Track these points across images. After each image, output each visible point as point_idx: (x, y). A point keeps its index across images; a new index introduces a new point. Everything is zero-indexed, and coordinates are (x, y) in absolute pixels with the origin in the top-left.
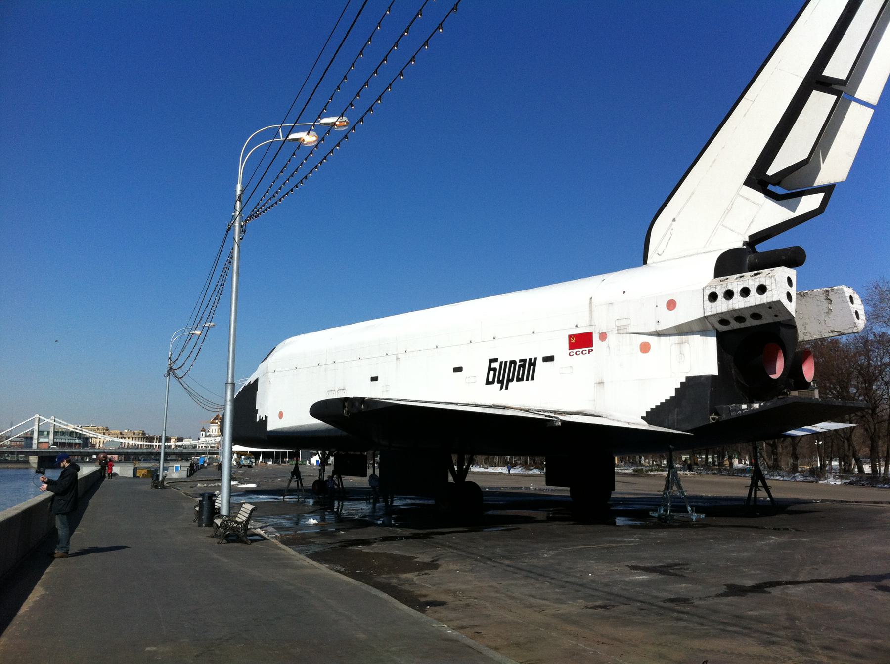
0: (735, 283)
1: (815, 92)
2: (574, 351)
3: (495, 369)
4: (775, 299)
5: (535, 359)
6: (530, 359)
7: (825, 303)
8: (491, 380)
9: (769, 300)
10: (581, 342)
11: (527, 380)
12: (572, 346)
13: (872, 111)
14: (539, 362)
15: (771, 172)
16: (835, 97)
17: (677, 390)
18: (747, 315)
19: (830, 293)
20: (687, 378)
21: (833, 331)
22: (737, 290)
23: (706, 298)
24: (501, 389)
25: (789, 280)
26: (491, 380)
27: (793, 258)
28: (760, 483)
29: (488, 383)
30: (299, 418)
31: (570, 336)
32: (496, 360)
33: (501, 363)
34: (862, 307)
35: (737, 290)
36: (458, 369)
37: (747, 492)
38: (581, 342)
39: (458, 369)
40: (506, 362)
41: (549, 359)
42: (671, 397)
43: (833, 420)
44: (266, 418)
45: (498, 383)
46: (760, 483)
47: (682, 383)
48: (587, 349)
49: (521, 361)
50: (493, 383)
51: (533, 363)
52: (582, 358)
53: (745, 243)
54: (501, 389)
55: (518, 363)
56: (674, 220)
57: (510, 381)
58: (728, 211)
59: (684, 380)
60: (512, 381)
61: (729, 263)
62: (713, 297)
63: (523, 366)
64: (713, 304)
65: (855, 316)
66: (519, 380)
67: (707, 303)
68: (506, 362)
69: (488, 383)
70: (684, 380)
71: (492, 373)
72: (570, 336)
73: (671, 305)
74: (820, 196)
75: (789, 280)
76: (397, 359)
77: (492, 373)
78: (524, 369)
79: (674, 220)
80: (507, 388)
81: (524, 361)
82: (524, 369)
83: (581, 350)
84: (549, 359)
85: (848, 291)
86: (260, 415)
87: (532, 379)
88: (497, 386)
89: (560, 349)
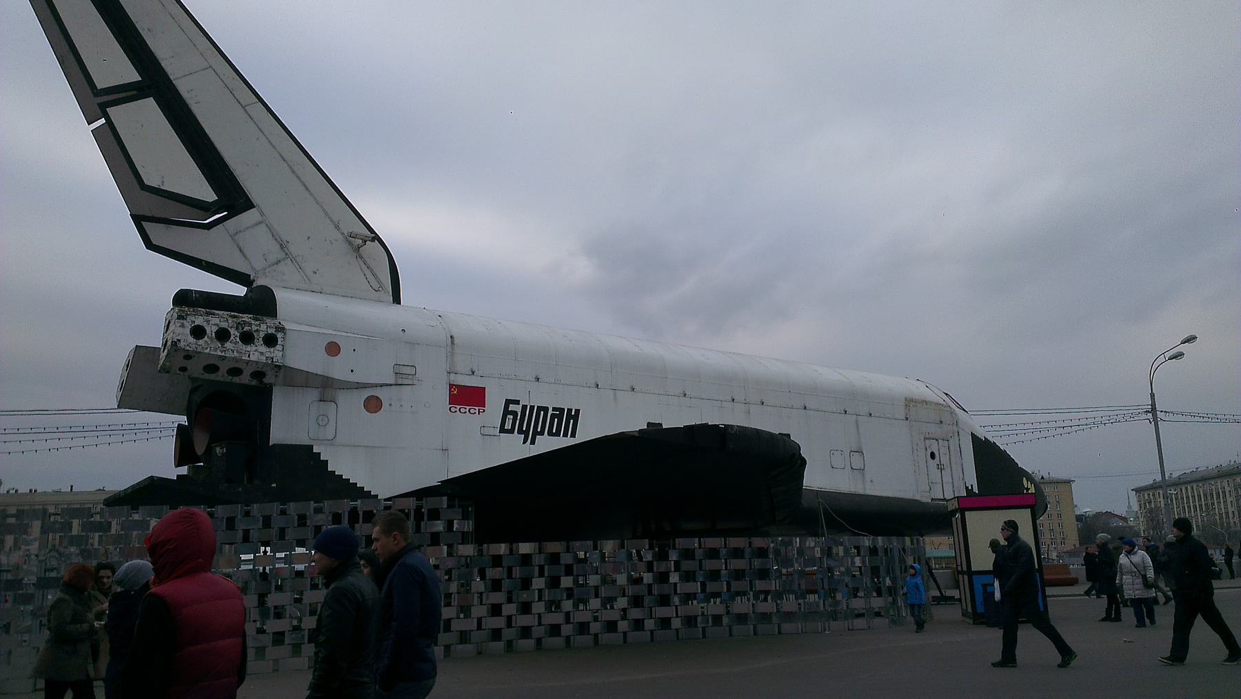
1: (151, 101)
3: (515, 413)
5: (577, 411)
6: (570, 410)
8: (508, 426)
10: (933, 456)
13: (1159, 478)
20: (804, 462)
22: (211, 330)
24: (524, 442)
26: (508, 426)
29: (503, 430)
32: (517, 402)
33: (524, 407)
35: (211, 330)
38: (933, 456)
49: (554, 409)
50: (511, 431)
54: (524, 442)
57: (536, 433)
60: (542, 433)
69: (503, 430)
73: (333, 349)
87: (1153, 621)
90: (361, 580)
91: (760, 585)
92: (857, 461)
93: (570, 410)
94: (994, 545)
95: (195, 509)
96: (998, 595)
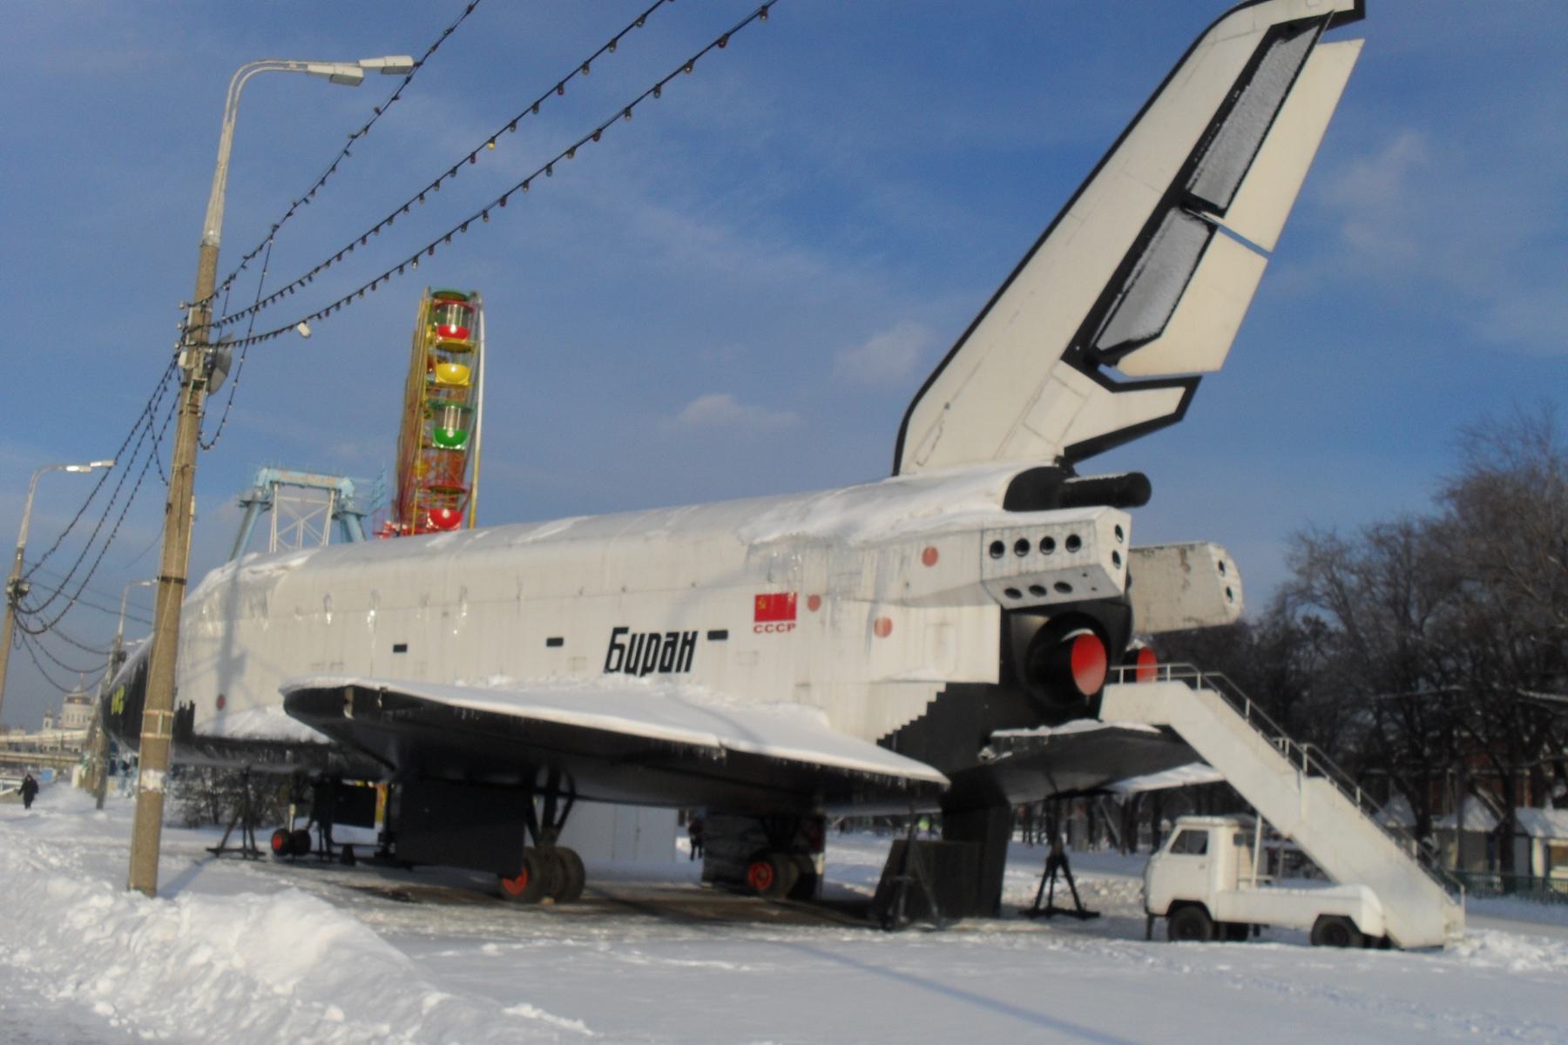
0: (1035, 523)
2: (764, 624)
3: (621, 647)
4: (1092, 561)
5: (695, 634)
6: (686, 634)
7: (1180, 571)
8: (613, 665)
9: (1084, 562)
10: (775, 609)
11: (678, 669)
12: (761, 615)
13: (1261, 262)
14: (702, 640)
15: (1104, 344)
17: (930, 705)
18: (1049, 584)
19: (1189, 553)
20: (950, 686)
21: (1190, 619)
22: (1035, 540)
23: (986, 549)
25: (1118, 531)
26: (613, 665)
27: (1127, 492)
28: (1060, 872)
29: (608, 669)
30: (262, 717)
31: (758, 598)
32: (624, 630)
33: (634, 636)
34: (1238, 582)
35: (1035, 540)
36: (555, 642)
39: (555, 642)
41: (718, 635)
42: (921, 718)
43: (1065, 736)
44: (192, 706)
46: (1060, 872)
48: (786, 623)
49: (669, 635)
51: (690, 641)
52: (774, 638)
53: (1058, 459)
55: (664, 640)
56: (947, 406)
58: (1035, 400)
61: (1029, 491)
62: (997, 548)
63: (672, 644)
64: (997, 562)
65: (1224, 594)
67: (988, 559)
68: (642, 636)
69: (608, 669)
71: (616, 653)
72: (758, 598)
74: (1178, 393)
75: (1118, 531)
76: (445, 614)
77: (616, 653)
78: (668, 653)
79: (947, 406)
81: (675, 635)
82: (668, 653)
83: (775, 623)
84: (718, 635)
85: (1216, 553)
87: (687, 669)
89: (738, 615)
90: (1478, 819)
91: (39, 866)
92: (306, 281)
93: (686, 634)
94: (229, 336)
95: (379, 826)
96: (349, 782)
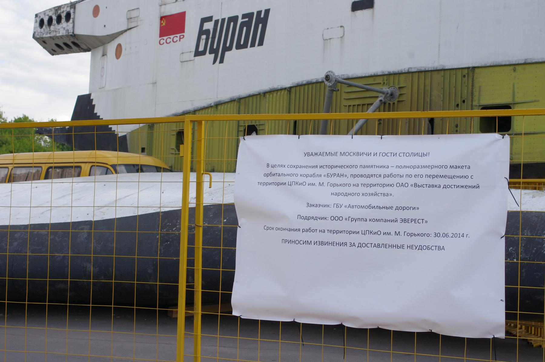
3: (207, 32)
5: (267, 12)
8: (201, 48)
16: (204, 29)
24: (214, 62)
26: (201, 48)
29: (198, 53)
33: (217, 22)
37: (179, 195)
40: (223, 20)
45: (210, 53)
47: (96, 113)
48: (178, 35)
49: (244, 16)
50: (203, 53)
54: (214, 62)
55: (240, 21)
59: (98, 115)
60: (230, 49)
66: (239, 47)
70: (98, 115)
71: (204, 37)
80: (222, 61)
86: (95, 112)
87: (261, 43)
88: (209, 57)
